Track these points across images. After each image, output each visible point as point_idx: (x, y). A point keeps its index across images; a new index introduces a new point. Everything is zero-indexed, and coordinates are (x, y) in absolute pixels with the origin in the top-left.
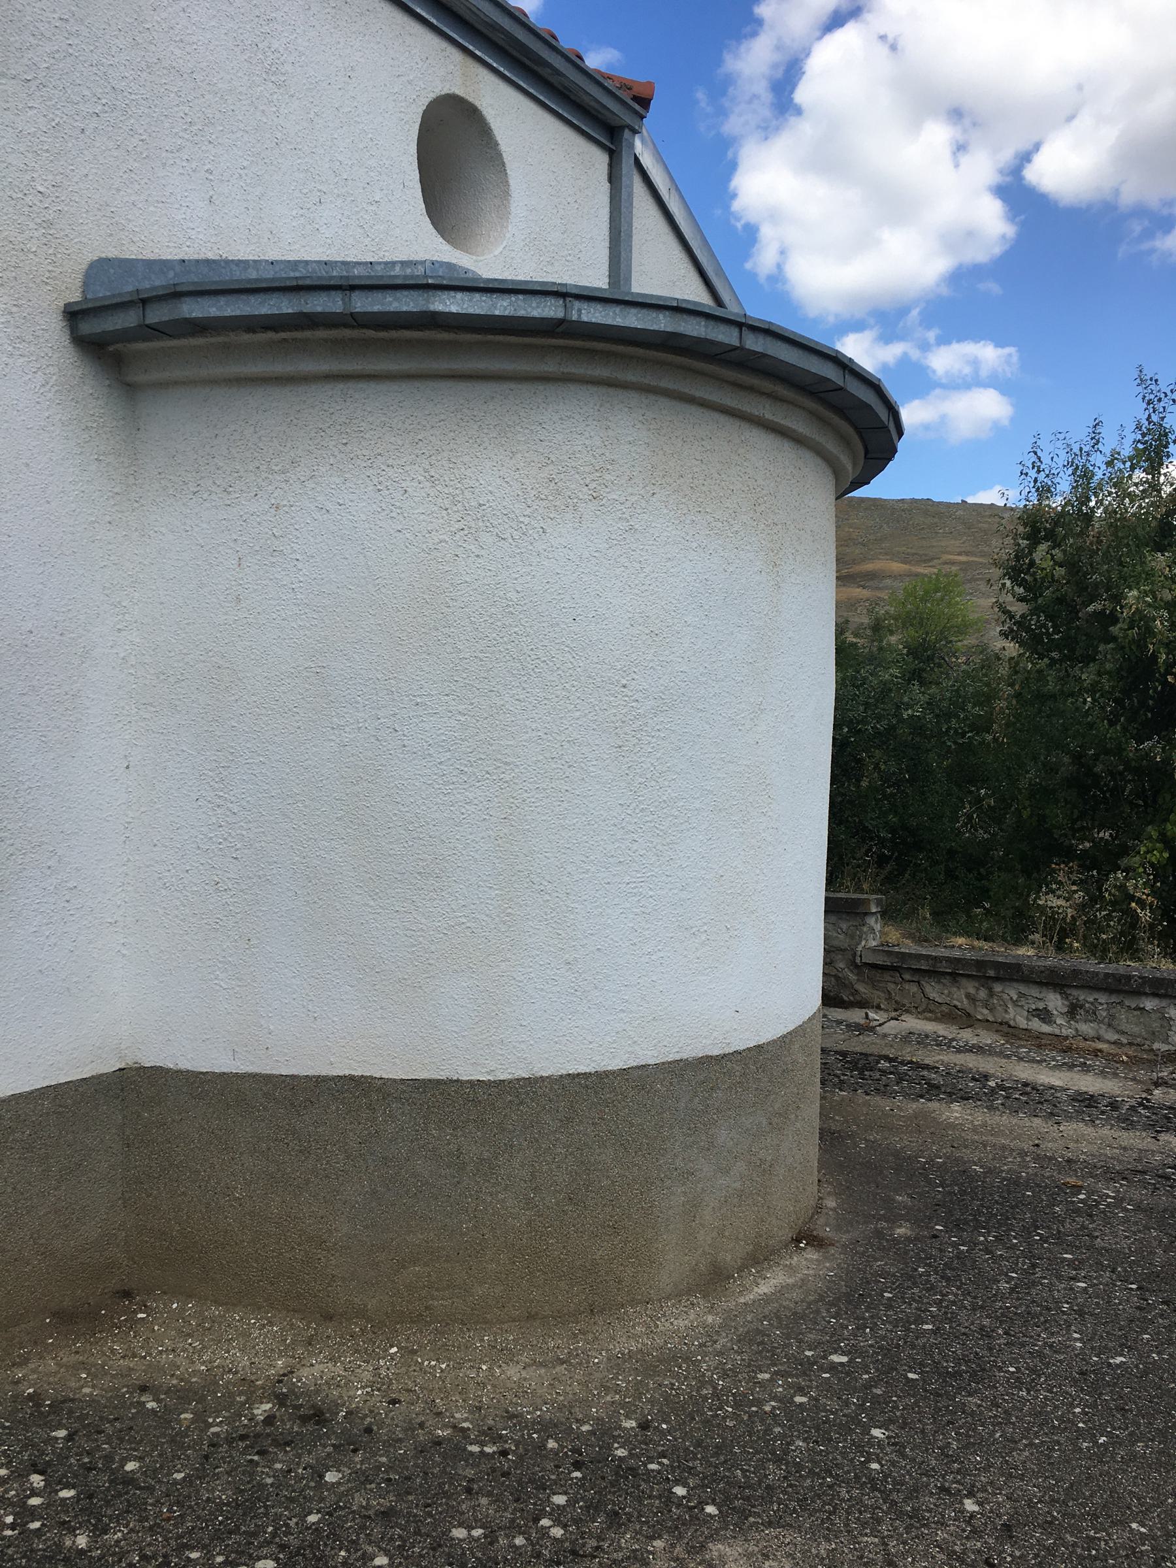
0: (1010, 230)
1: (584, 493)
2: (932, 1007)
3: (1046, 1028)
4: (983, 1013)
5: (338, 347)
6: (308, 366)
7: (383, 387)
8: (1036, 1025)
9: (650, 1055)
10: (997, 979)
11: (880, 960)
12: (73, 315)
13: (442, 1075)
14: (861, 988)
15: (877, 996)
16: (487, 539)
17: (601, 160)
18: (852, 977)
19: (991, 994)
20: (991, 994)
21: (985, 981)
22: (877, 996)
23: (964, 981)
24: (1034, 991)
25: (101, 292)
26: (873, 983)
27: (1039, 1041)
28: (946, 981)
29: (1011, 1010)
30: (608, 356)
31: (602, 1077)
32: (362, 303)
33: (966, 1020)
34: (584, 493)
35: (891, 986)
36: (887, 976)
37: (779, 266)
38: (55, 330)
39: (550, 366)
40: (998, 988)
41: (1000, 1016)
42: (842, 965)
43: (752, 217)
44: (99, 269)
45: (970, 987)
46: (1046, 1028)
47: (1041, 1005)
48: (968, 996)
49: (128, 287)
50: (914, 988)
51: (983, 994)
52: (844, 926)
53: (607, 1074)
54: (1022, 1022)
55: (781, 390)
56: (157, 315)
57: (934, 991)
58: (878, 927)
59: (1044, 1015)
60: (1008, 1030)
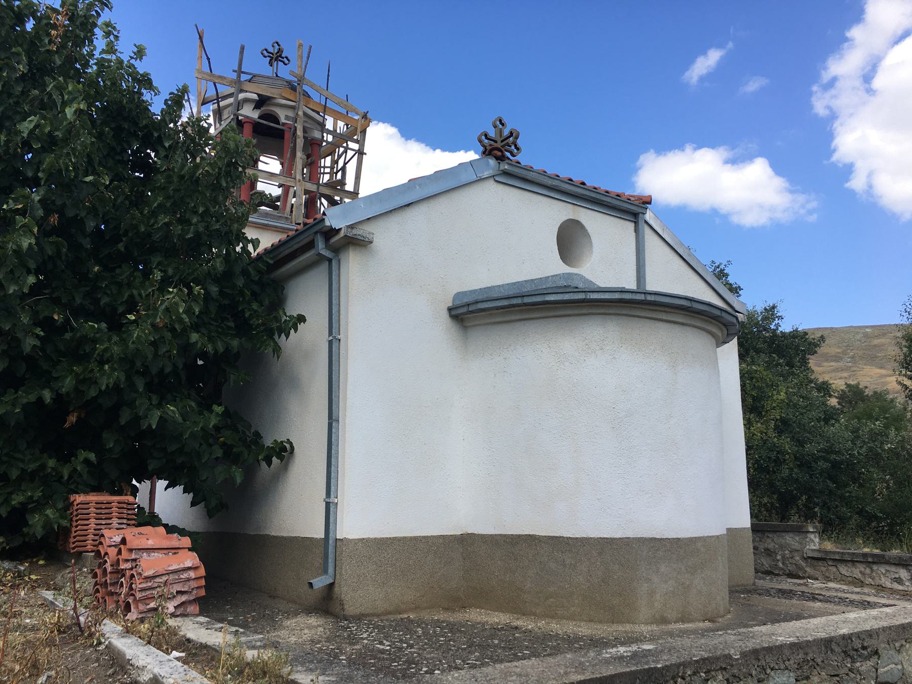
0: (27, 516)
1: (598, 348)
2: (844, 578)
3: (901, 588)
4: (869, 581)
5: (521, 311)
6: (513, 318)
7: (536, 321)
8: (896, 586)
9: (630, 534)
10: (874, 563)
11: (816, 555)
12: (450, 310)
13: (557, 535)
14: (808, 569)
15: (817, 574)
16: (567, 364)
17: (631, 226)
18: (804, 564)
19: (872, 570)
20: (872, 570)
21: (869, 564)
22: (817, 574)
23: (858, 565)
24: (893, 569)
25: (458, 303)
26: (814, 567)
27: (893, 591)
28: (850, 565)
29: (883, 579)
30: (603, 306)
31: (612, 539)
32: (527, 300)
33: (861, 584)
34: (598, 348)
35: (823, 569)
36: (820, 563)
37: (870, 186)
38: (445, 314)
39: (584, 311)
40: (875, 567)
41: (878, 582)
42: (798, 558)
43: (847, 160)
44: (457, 295)
45: (861, 567)
46: (901, 588)
47: (897, 576)
48: (861, 572)
49: (466, 300)
50: (834, 569)
51: (868, 571)
52: (797, 538)
53: (615, 539)
54: (888, 584)
55: (667, 309)
56: (471, 308)
57: (844, 570)
58: (817, 540)
59: (899, 581)
60: (880, 588)
